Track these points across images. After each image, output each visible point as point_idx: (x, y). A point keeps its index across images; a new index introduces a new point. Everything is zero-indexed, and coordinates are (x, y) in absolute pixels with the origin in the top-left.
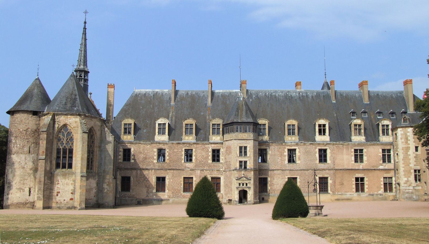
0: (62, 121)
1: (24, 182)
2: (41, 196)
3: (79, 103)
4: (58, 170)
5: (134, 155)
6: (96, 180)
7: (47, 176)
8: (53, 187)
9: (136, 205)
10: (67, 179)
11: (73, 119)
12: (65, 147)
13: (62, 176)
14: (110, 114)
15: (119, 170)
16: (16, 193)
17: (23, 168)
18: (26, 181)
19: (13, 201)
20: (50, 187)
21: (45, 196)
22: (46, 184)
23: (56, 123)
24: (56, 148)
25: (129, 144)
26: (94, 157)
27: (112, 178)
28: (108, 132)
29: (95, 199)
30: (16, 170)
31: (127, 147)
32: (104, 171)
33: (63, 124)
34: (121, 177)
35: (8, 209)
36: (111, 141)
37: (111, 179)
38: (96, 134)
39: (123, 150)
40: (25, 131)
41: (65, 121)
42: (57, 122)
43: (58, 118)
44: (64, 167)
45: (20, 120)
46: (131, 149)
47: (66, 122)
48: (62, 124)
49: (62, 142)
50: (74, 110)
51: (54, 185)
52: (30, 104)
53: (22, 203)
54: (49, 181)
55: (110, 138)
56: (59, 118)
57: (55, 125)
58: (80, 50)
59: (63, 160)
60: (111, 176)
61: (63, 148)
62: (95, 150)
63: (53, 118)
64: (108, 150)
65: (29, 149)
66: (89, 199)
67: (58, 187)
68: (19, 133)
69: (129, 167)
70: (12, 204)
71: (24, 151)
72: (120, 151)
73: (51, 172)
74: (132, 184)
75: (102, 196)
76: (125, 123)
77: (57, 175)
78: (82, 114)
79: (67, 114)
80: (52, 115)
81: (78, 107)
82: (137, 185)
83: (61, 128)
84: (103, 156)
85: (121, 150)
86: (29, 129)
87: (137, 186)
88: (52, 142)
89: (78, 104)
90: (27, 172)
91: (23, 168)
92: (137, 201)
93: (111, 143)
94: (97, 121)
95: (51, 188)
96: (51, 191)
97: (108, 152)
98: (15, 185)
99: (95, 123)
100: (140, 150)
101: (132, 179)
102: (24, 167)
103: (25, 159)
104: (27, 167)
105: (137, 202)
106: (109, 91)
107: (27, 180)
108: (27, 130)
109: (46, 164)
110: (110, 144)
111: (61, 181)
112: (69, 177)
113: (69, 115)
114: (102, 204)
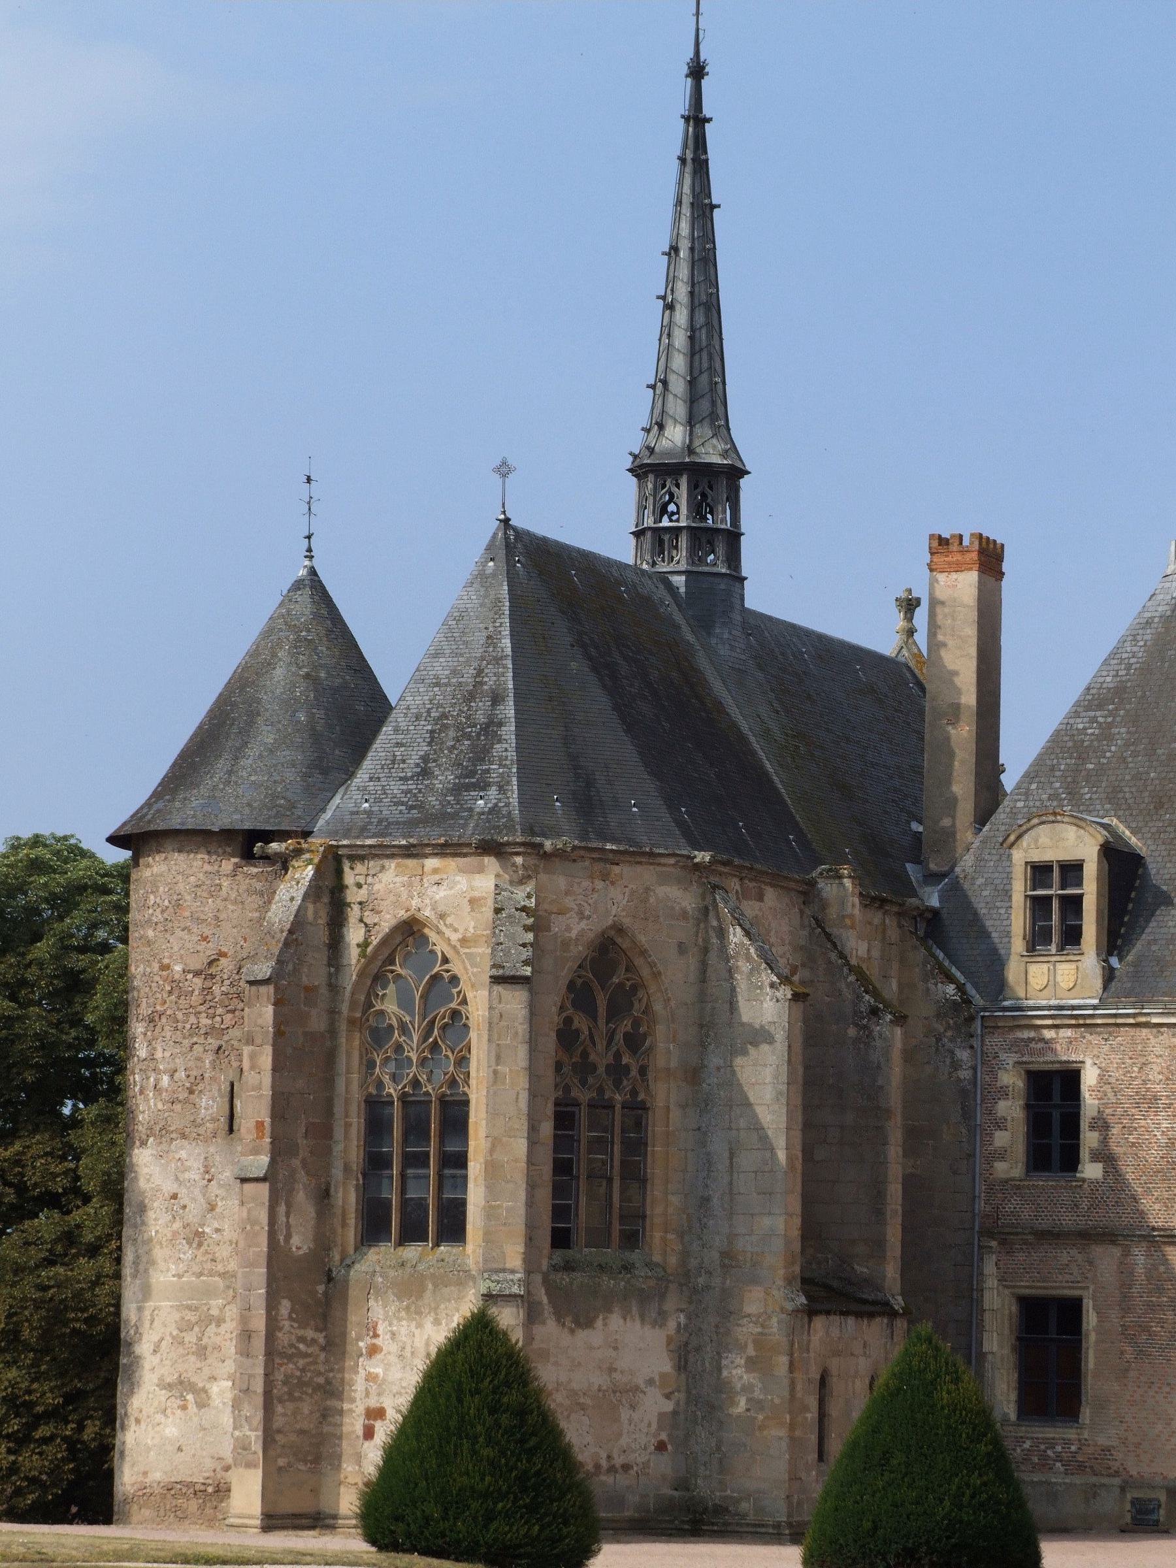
0: (388, 902)
1: (205, 1341)
2: (253, 1435)
3: (512, 754)
4: (373, 1250)
5: (1102, 1124)
6: (672, 1325)
7: (290, 1299)
8: (339, 1376)
9: (1123, 1531)
10: (430, 1319)
11: (458, 878)
12: (416, 1083)
13: (399, 1298)
14: (950, 784)
15: (994, 1244)
16: (159, 1417)
17: (197, 1238)
18: (217, 1334)
19: (145, 1473)
20: (320, 1374)
21: (278, 1437)
22: (283, 1355)
23: (354, 913)
24: (357, 1095)
25: (1069, 1033)
26: (649, 1154)
27: (782, 1310)
28: (748, 958)
29: (664, 1466)
30: (159, 1253)
31: (1049, 1057)
32: (729, 1258)
33: (394, 922)
34: (1014, 1301)
35: (124, 1523)
36: (772, 1029)
37: (775, 1320)
38: (656, 975)
39: (1020, 1084)
40: (197, 974)
41: (404, 896)
42: (356, 908)
43: (361, 879)
44: (412, 1233)
45: (166, 903)
46: (1082, 1071)
47: (415, 903)
48: (386, 922)
49: (399, 1048)
50: (471, 810)
51: (349, 1363)
52: (228, 783)
53: (198, 1487)
54: (310, 1334)
55: (765, 1005)
56: (370, 879)
57: (345, 929)
58: (664, 298)
59: (411, 1184)
60: (775, 1292)
61: (403, 1097)
62: (660, 1103)
63: (328, 882)
64: (752, 1100)
65: (227, 1106)
66: (604, 1463)
67: (371, 1378)
68: (165, 995)
69: (1068, 1220)
70: (145, 1494)
71: (199, 1121)
72: (1004, 1093)
73: (330, 1270)
74: (1091, 1360)
75: (719, 1449)
76: (1037, 856)
77: (369, 1289)
78: (508, 844)
79: (414, 846)
80: (316, 861)
81: (501, 789)
82: (1127, 1370)
83: (386, 953)
84: (718, 1146)
85: (1012, 1079)
86: (223, 961)
87: (1132, 1374)
88: (330, 1058)
89: (500, 765)
90: (220, 1268)
91: (197, 1238)
92: (1129, 1496)
93: (769, 1039)
94: (664, 879)
95: (328, 1382)
96: (328, 1403)
97: (753, 1111)
98: (155, 1360)
99: (646, 900)
100: (1145, 1082)
101: (1090, 1319)
102: (197, 1234)
103: (207, 1176)
104: (217, 1230)
105: (1128, 1507)
106: (940, 594)
107: (219, 1321)
108: (213, 970)
109: (282, 1209)
110: (765, 1047)
111: (393, 1334)
112: (442, 1306)
113: (428, 850)
114: (720, 1510)
